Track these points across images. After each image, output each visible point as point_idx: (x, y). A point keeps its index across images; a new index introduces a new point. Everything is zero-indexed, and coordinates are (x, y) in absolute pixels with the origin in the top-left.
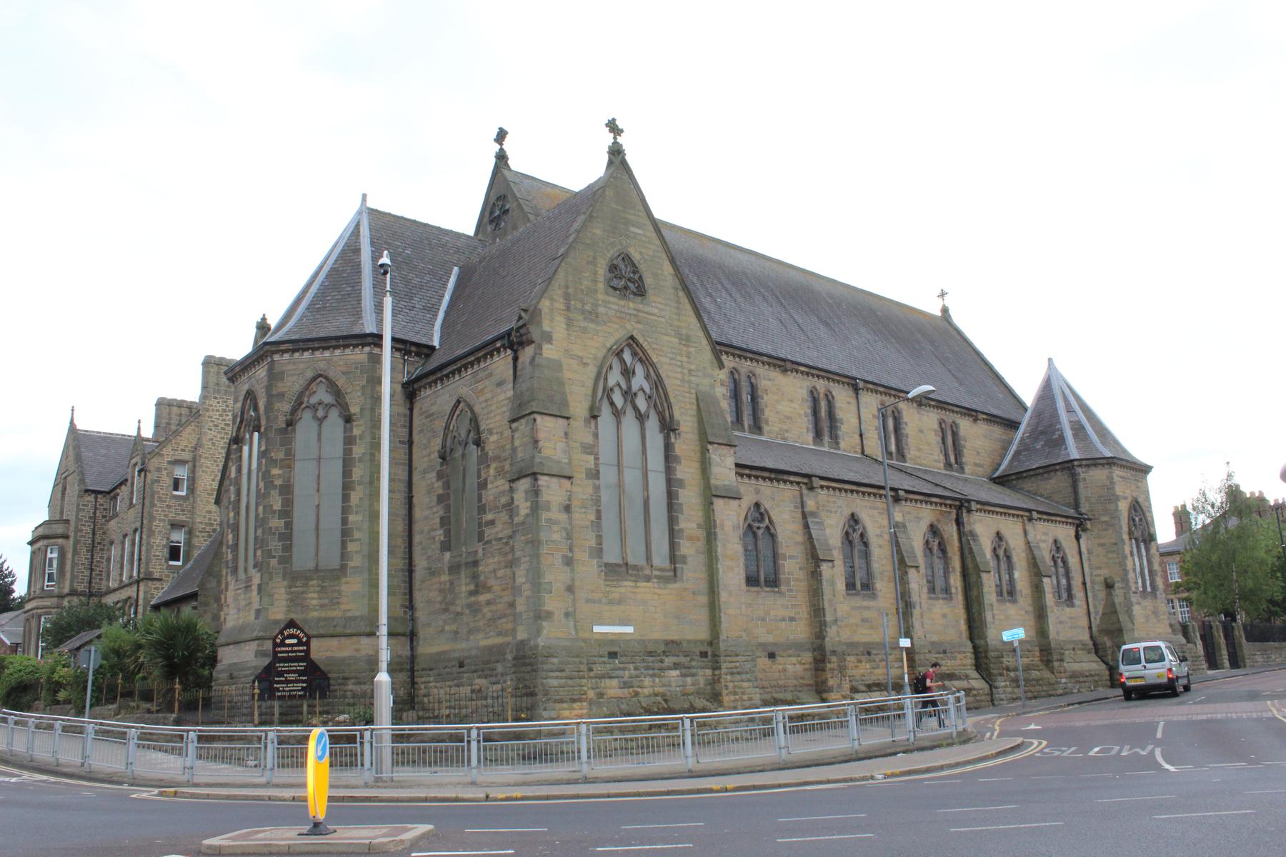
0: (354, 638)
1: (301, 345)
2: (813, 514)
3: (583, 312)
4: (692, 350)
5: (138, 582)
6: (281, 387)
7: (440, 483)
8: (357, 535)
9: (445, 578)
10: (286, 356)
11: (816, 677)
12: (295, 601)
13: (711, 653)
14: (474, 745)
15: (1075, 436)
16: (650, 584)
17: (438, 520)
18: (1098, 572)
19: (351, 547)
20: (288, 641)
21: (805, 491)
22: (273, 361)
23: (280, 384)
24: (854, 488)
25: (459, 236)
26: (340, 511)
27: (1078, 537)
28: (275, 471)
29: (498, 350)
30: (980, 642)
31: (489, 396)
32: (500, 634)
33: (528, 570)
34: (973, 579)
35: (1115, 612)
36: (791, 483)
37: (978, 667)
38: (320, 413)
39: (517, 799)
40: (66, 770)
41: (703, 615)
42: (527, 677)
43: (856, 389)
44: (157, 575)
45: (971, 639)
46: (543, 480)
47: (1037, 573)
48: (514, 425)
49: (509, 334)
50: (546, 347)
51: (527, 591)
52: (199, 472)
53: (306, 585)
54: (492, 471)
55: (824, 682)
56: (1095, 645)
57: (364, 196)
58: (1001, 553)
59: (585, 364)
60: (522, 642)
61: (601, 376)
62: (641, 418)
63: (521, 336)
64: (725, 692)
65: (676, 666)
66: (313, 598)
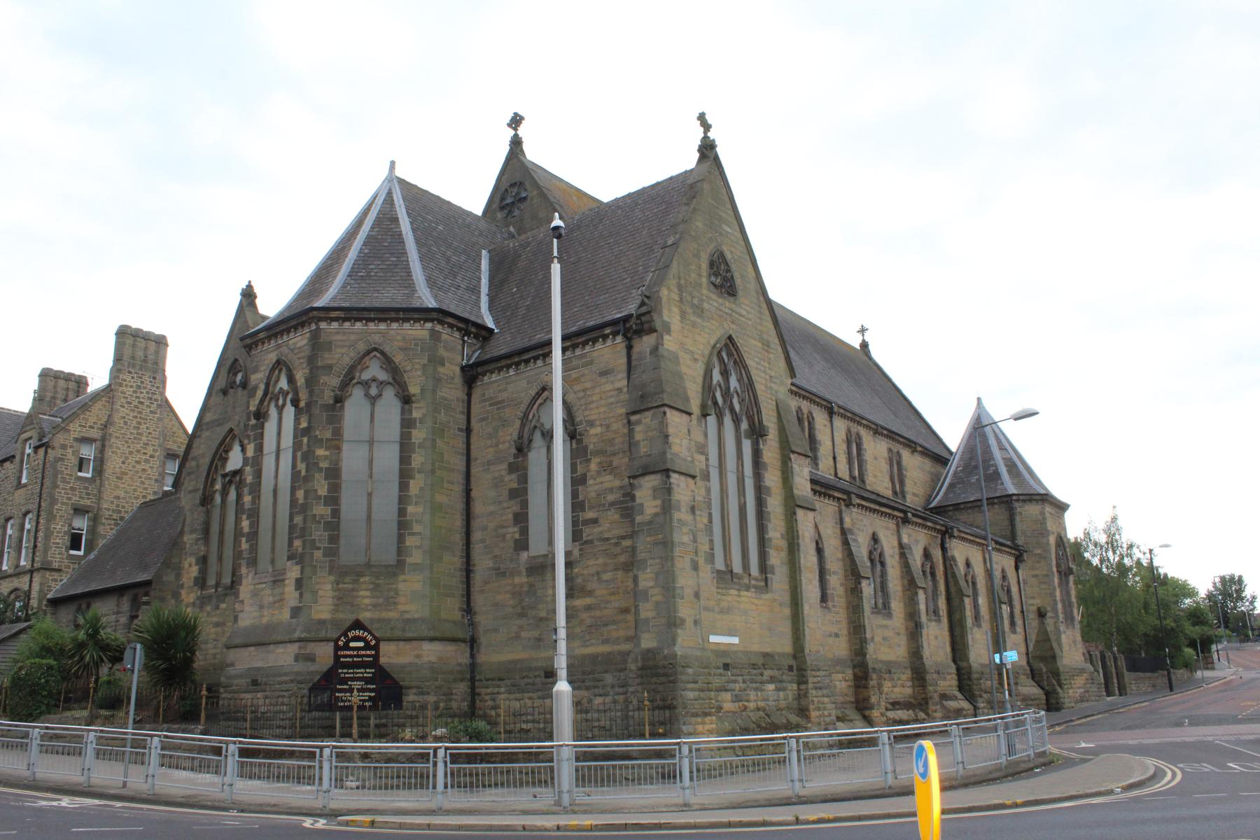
0: (415, 643)
1: (355, 314)
2: (850, 530)
3: (693, 306)
4: (771, 356)
5: (31, 572)
6: (327, 358)
7: (514, 476)
8: (417, 528)
9: (521, 579)
10: (335, 325)
11: (856, 693)
12: (343, 599)
13: (798, 666)
14: (440, 766)
15: (1009, 472)
16: (748, 594)
17: (511, 516)
18: (1031, 601)
19: (410, 541)
20: (352, 644)
21: (843, 508)
22: (318, 328)
23: (326, 355)
24: (877, 507)
25: (469, 214)
26: (396, 501)
27: (1017, 568)
28: (320, 452)
29: (605, 337)
30: (963, 664)
31: (588, 385)
32: (606, 642)
33: (657, 574)
34: (956, 602)
35: (1049, 640)
36: (834, 498)
37: (961, 688)
38: (374, 391)
39: (829, 821)
40: (112, 792)
41: (786, 628)
42: (660, 688)
43: (831, 413)
44: (55, 565)
45: (954, 661)
46: (674, 477)
47: (994, 602)
48: (633, 418)
49: (626, 319)
50: (666, 337)
51: (656, 595)
52: (108, 453)
53: (356, 581)
54: (593, 466)
55: (867, 699)
56: (1032, 670)
57: (393, 164)
58: (969, 578)
59: (696, 360)
60: (649, 651)
61: (708, 374)
62: (736, 421)
63: (642, 324)
64: (812, 707)
65: (772, 680)
66: (365, 597)
